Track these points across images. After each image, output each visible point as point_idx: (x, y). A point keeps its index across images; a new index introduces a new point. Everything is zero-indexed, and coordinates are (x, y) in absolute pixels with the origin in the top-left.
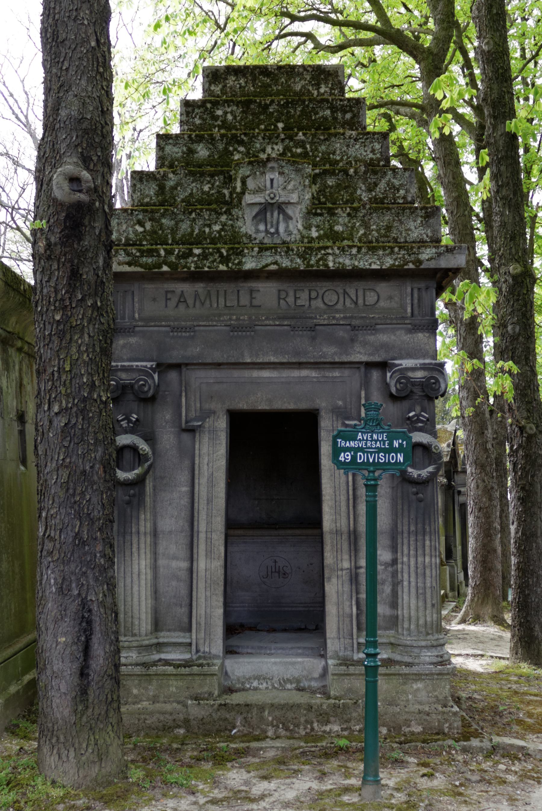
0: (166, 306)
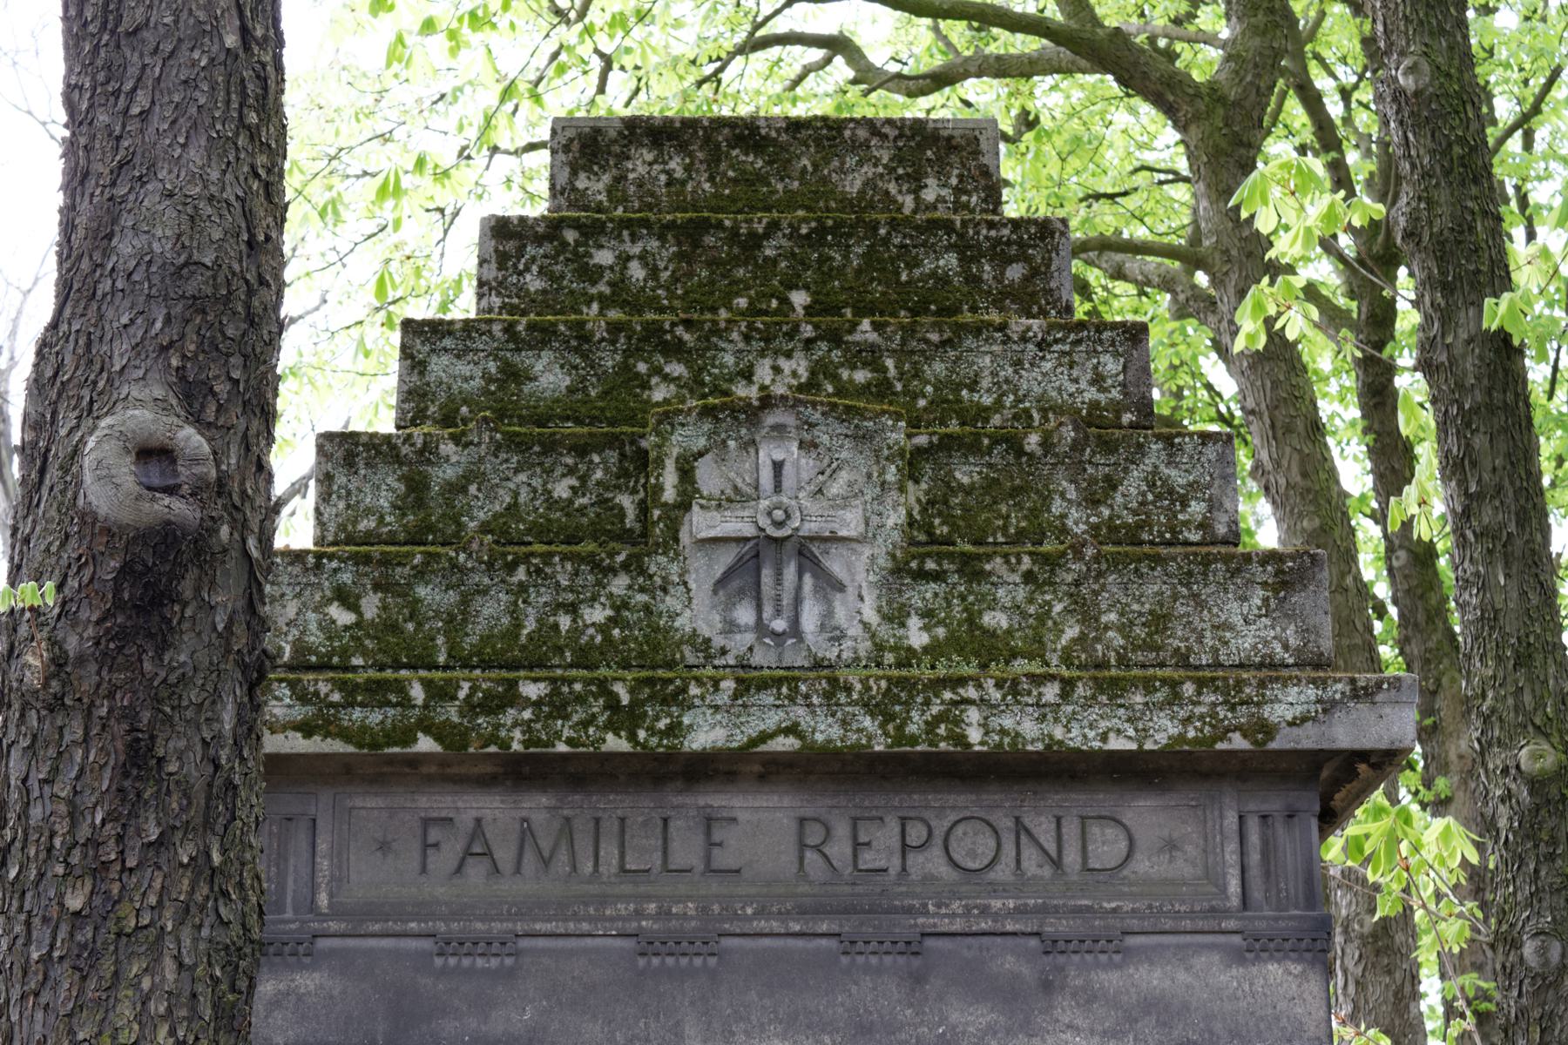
0: (424, 869)
